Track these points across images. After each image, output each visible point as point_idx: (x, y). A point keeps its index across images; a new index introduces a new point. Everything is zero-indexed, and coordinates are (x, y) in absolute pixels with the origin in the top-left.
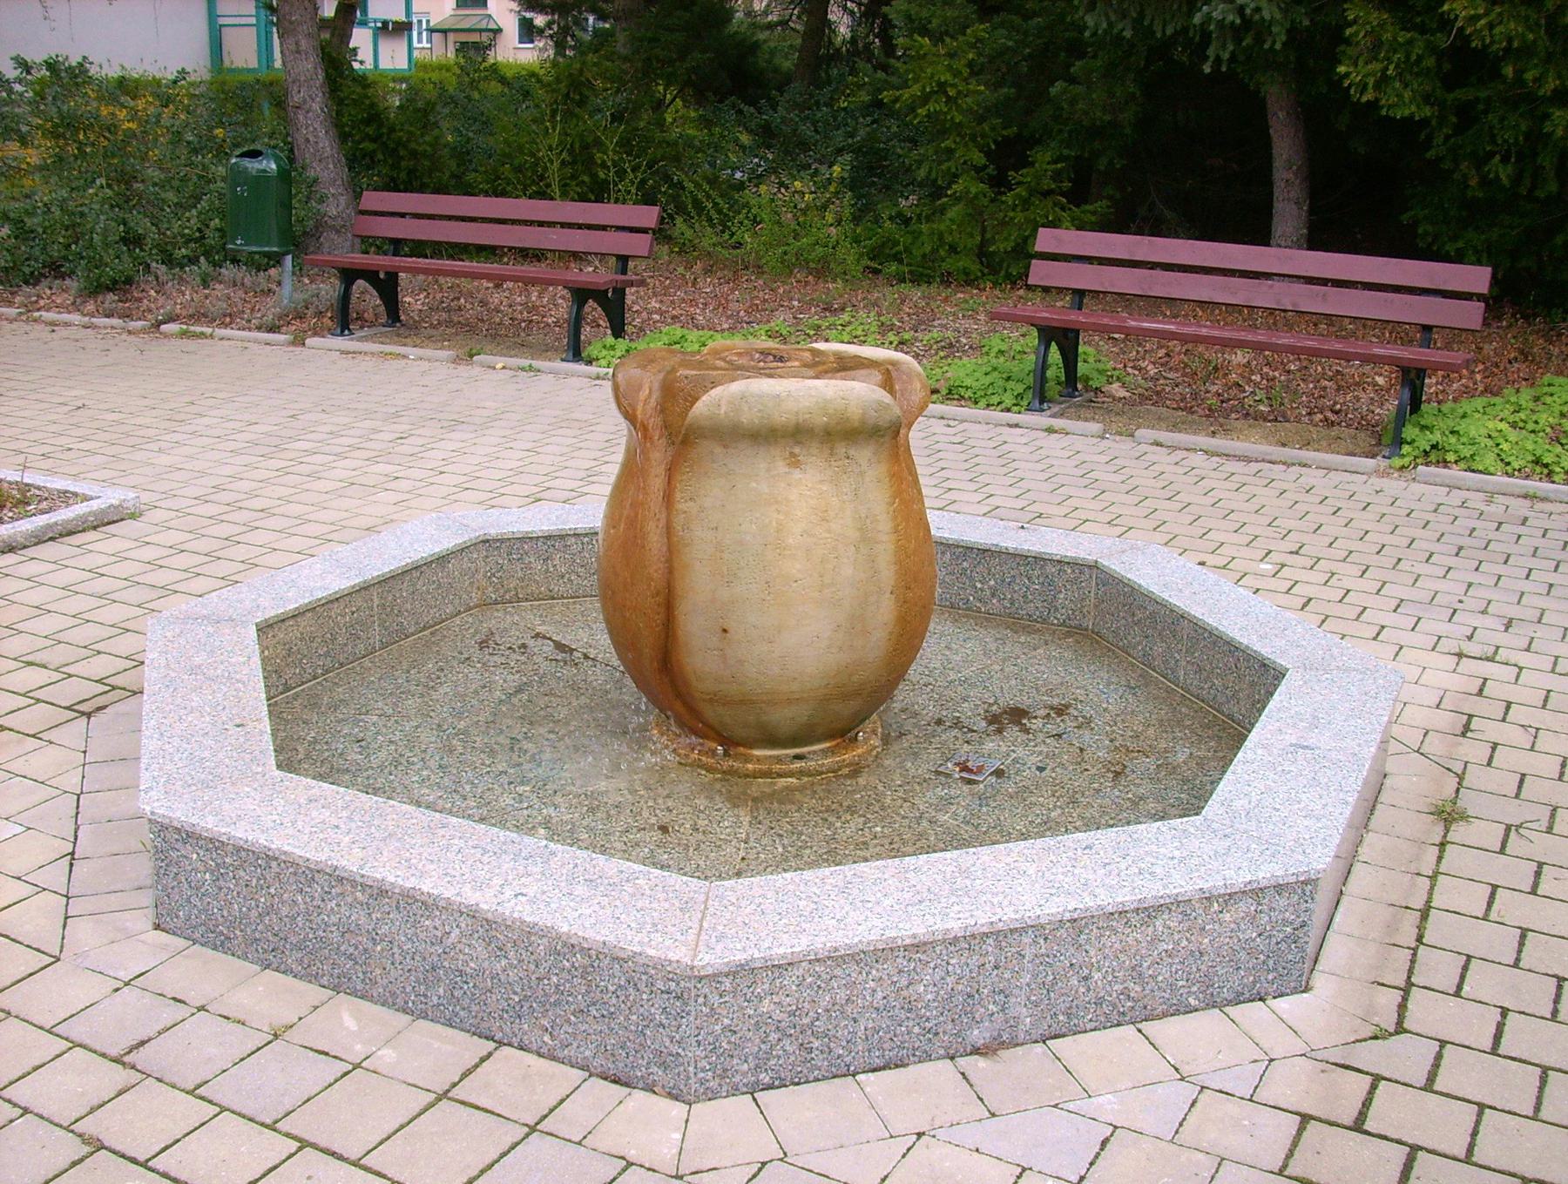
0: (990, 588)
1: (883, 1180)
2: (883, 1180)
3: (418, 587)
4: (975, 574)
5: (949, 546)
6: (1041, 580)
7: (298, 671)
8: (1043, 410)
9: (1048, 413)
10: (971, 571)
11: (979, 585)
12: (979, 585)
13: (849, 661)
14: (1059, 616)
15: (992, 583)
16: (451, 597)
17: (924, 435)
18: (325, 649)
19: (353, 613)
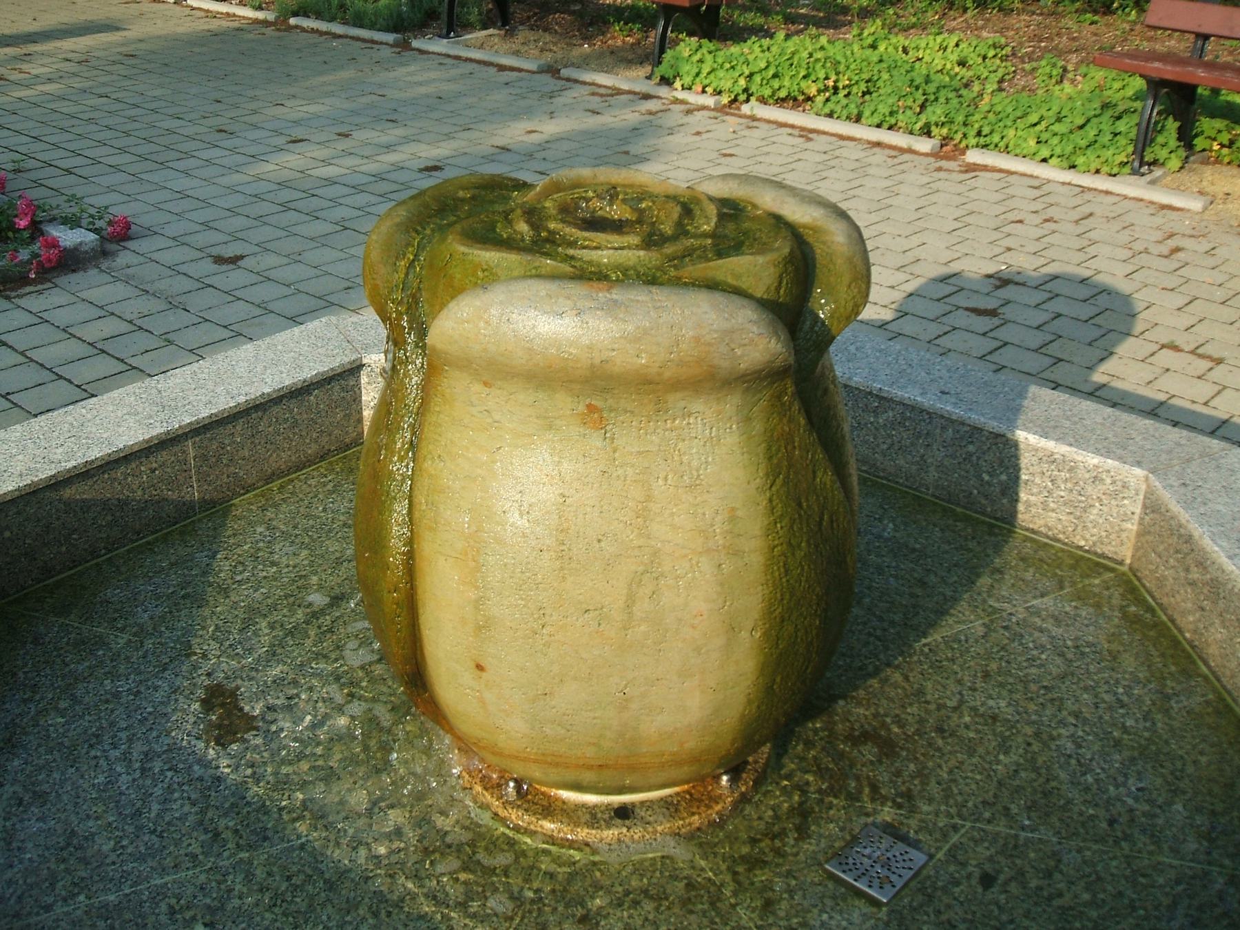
0: (1000, 483)
1: (1237, 390)
2: (1237, 390)
3: (260, 428)
4: (981, 462)
5: (952, 421)
6: (1069, 485)
7: (64, 549)
8: (1143, 175)
9: (1148, 178)
10: (979, 458)
11: (986, 477)
12: (986, 477)
13: (679, 725)
14: (1088, 536)
15: (1004, 477)
16: (315, 435)
17: (1001, 197)
18: (109, 518)
19: (153, 471)
